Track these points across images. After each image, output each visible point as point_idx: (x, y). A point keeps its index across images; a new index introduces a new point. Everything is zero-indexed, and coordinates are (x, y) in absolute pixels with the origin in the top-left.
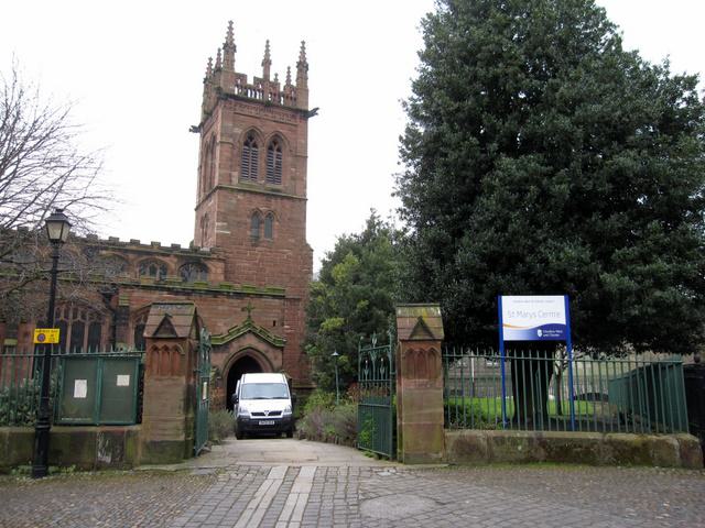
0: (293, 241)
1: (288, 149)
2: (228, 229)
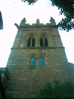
0: (59, 64)
1: (49, 35)
2: (14, 63)
